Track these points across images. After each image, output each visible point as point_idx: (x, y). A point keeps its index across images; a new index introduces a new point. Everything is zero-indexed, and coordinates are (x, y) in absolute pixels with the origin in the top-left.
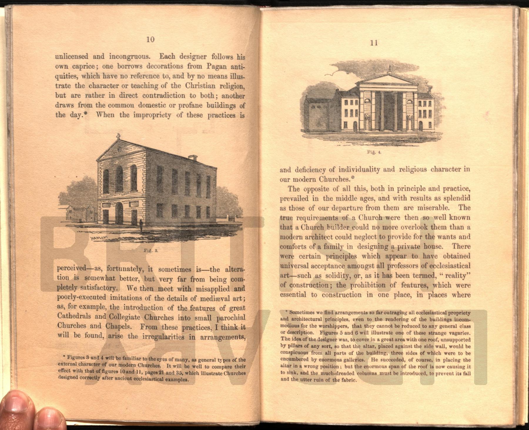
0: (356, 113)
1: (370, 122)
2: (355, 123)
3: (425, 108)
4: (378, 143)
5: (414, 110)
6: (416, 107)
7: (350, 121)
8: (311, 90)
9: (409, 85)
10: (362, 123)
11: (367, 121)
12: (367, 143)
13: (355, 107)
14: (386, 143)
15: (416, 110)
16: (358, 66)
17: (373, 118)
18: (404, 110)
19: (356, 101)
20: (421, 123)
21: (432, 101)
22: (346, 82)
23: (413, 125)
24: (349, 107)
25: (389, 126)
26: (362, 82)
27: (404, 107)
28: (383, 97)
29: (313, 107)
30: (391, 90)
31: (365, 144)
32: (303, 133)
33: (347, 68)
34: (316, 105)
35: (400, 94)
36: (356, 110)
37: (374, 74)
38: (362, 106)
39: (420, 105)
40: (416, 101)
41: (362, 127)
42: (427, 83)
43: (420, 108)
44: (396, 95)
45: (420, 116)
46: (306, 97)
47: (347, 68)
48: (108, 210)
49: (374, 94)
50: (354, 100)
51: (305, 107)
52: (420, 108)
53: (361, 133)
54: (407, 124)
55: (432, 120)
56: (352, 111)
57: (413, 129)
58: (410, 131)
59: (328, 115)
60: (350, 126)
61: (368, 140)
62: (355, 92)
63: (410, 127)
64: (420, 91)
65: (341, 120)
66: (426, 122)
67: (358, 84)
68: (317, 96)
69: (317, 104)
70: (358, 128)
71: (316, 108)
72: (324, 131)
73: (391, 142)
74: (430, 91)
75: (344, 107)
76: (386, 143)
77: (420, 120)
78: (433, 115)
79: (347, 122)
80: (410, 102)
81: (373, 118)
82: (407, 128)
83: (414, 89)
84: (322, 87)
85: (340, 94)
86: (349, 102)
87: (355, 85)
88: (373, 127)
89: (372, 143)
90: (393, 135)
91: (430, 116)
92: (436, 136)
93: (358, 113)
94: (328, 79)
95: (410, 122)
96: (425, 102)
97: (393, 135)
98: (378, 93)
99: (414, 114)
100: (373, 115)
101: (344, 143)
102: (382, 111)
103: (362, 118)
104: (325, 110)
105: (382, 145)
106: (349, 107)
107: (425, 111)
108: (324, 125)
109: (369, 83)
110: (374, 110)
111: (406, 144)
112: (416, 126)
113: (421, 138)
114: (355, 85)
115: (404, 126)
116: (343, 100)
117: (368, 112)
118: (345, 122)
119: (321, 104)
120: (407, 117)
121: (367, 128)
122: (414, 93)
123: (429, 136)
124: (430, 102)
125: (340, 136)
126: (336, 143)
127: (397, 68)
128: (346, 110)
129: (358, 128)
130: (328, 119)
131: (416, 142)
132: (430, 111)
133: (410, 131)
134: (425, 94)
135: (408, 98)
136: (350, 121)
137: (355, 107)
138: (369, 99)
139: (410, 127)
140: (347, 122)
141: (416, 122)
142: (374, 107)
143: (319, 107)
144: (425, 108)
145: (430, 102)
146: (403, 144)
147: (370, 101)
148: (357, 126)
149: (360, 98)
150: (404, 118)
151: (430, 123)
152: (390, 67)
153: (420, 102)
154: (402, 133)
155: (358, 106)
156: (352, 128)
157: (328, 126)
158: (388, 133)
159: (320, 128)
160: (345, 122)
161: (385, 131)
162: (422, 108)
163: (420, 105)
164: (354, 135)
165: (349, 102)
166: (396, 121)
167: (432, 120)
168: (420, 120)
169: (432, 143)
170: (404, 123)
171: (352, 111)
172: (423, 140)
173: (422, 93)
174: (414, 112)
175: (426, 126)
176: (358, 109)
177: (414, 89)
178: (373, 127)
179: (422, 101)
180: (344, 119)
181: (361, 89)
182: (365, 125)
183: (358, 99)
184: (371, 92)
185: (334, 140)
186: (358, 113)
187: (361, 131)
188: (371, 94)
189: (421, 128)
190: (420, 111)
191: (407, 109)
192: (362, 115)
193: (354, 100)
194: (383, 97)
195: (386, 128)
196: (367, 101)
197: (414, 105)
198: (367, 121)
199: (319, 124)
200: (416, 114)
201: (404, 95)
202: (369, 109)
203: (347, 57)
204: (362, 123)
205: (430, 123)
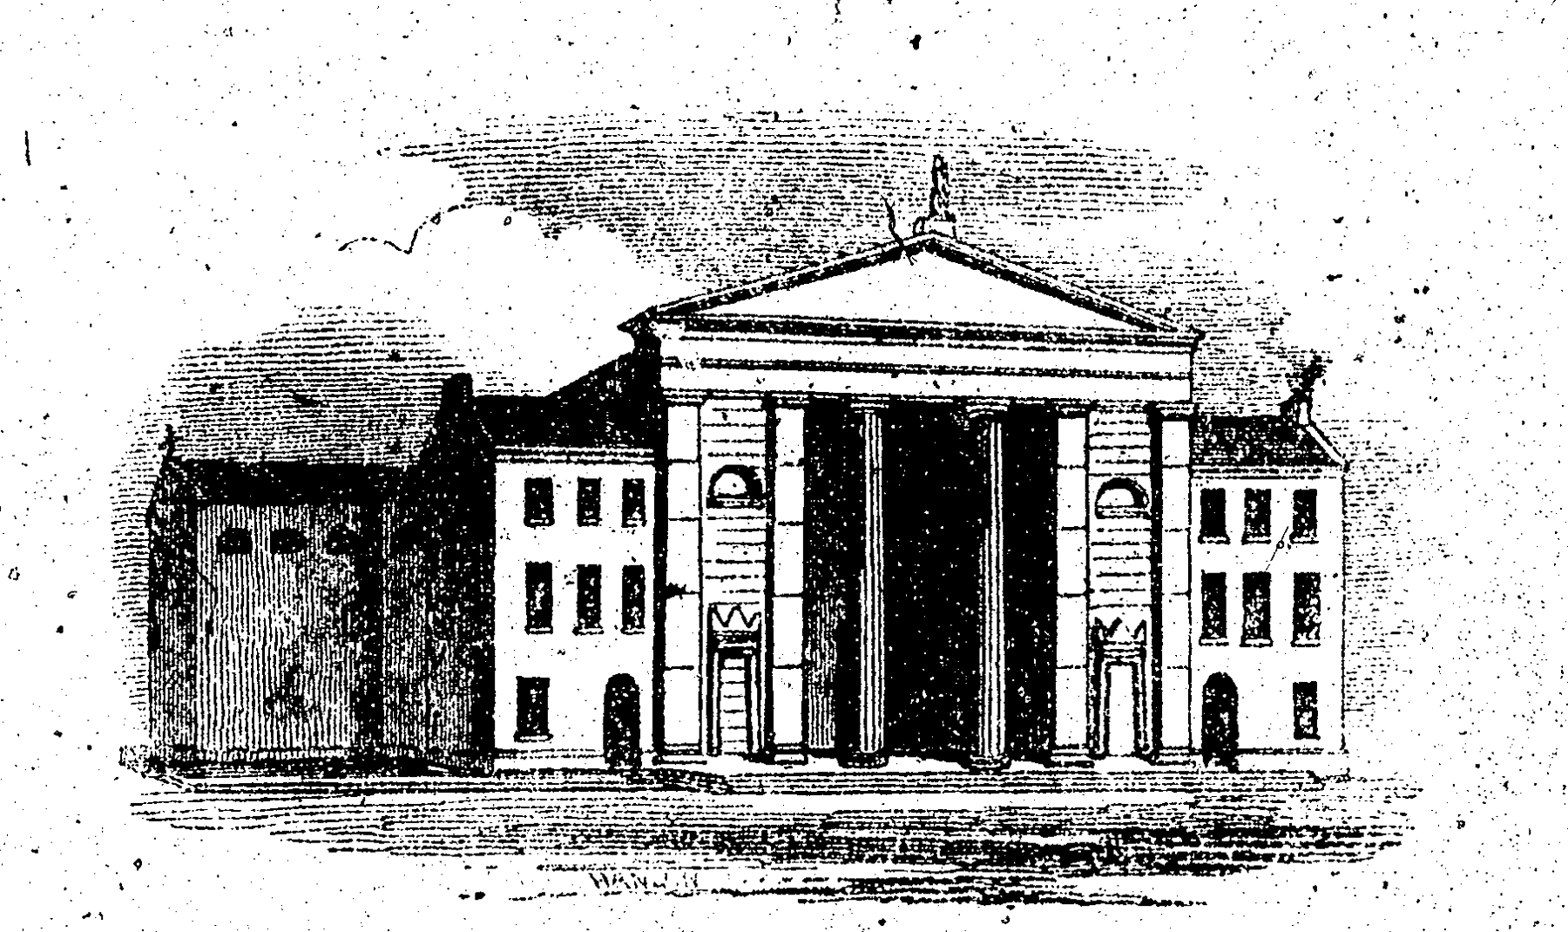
0: (631, 600)
1: (761, 684)
2: (620, 690)
3: (1255, 558)
4: (834, 873)
5: (1156, 573)
6: (1173, 545)
7: (578, 669)
8: (208, 384)
9: (1111, 341)
10: (682, 691)
11: (732, 672)
12: (740, 872)
13: (617, 546)
14: (907, 871)
15: (1173, 579)
16: (656, 163)
17: (788, 642)
18: (1069, 576)
19: (633, 490)
20: (1221, 693)
21: (1327, 486)
22: (539, 318)
23: (1151, 704)
24: (565, 544)
25: (931, 720)
26: (686, 313)
27: (1069, 549)
28: (873, 451)
29: (235, 542)
30: (950, 388)
31: (708, 880)
32: (142, 785)
33: (547, 185)
34: (263, 522)
35: (1033, 427)
36: (632, 574)
37: (798, 240)
38: (680, 538)
39: (1213, 525)
40: (1176, 484)
41: (683, 725)
42: (1273, 328)
43: (1212, 557)
44: (995, 434)
45: (1214, 626)
46: (171, 440)
47: (547, 185)
48: (1246, 576)
49: (792, 425)
50: (612, 480)
51: (158, 544)
52: (1212, 557)
53: (670, 781)
54: (1096, 702)
55: (1317, 664)
56: (589, 576)
57: (1150, 750)
58: (1120, 759)
59: (364, 613)
60: (577, 722)
61: (733, 843)
62: (621, 405)
63: (1122, 737)
64: (1217, 401)
65: (484, 664)
66: (1264, 679)
67: (641, 327)
68: (267, 435)
69: (275, 518)
70: (646, 741)
71: (261, 546)
72: (337, 767)
73: (949, 871)
74: (1302, 396)
75: (515, 545)
76: (907, 871)
77: (1212, 659)
78: (1329, 620)
79: (543, 684)
80: (1124, 497)
81: (788, 642)
82: (1097, 743)
83: (1162, 376)
84: (298, 372)
85: (479, 425)
86: (565, 501)
87: (627, 344)
88: (788, 729)
89: (774, 878)
90: (975, 803)
91: (1303, 626)
92: (1358, 808)
93: (647, 593)
94: (361, 290)
95: (1121, 677)
96: (1260, 504)
97: (975, 803)
98: (830, 421)
99: (1156, 609)
100: (789, 616)
101: (516, 871)
102: (871, 580)
103: (684, 643)
104: (339, 572)
105: (866, 887)
106: (565, 544)
107: (1257, 583)
108: (339, 708)
109: (722, 326)
110: (790, 575)
111: (1086, 886)
112: (1181, 723)
113: (1220, 832)
114: (627, 344)
115: (1071, 725)
116: (510, 480)
117: (735, 593)
118: (524, 684)
119: (298, 520)
120: (1098, 638)
121: (734, 738)
122: (1155, 415)
123: (1295, 811)
124: (1305, 502)
125: (484, 809)
126: (447, 871)
127: (1008, 188)
128: (538, 574)
129: (646, 741)
130: (374, 646)
131: (1172, 867)
132: (1306, 585)
133: (1120, 759)
134: (1258, 422)
135: (1105, 465)
136: (578, 669)
137: (617, 546)
138: (746, 473)
139: (1122, 737)
140: (543, 684)
141: (1173, 684)
142: (790, 545)
143: (286, 541)
144: (1255, 558)
145: (1305, 502)
146: (1060, 884)
147: (759, 493)
148: (633, 722)
149: (662, 463)
150: (1070, 644)
151: (1305, 692)
152: (940, 169)
153: (1213, 503)
154: (1055, 788)
155: (646, 533)
156: (596, 739)
157: (367, 708)
158: (927, 785)
159: (298, 739)
160: (524, 684)
161: (898, 764)
162: (1233, 559)
163: (1213, 525)
164: (611, 807)
165: (565, 501)
166: (994, 670)
167: (1317, 664)
168: (1212, 659)
169: (1319, 868)
170: (1070, 691)
171: (589, 576)
172: (1248, 841)
173: (1232, 421)
174: (1157, 593)
175: (1263, 719)
176: (647, 560)
177: (1162, 376)
178: (788, 729)
179: (1235, 492)
180: (516, 653)
181: (670, 379)
182: (709, 706)
183: (648, 474)
184: (769, 402)
185: (436, 847)
186: (647, 593)
187: (672, 763)
188: (772, 424)
189: (1220, 743)
190: (1214, 584)
191: (1094, 564)
192: (682, 618)
193: (612, 480)
194: (873, 451)
195: (897, 742)
196: (732, 484)
197: (1156, 531)
198: (732, 672)
199: (286, 697)
200: (1173, 610)
201: (1070, 433)
202: (741, 560)
203: (542, 97)
204: (682, 691)
205: (1305, 692)
